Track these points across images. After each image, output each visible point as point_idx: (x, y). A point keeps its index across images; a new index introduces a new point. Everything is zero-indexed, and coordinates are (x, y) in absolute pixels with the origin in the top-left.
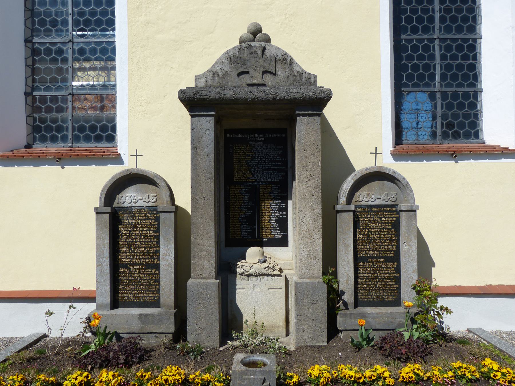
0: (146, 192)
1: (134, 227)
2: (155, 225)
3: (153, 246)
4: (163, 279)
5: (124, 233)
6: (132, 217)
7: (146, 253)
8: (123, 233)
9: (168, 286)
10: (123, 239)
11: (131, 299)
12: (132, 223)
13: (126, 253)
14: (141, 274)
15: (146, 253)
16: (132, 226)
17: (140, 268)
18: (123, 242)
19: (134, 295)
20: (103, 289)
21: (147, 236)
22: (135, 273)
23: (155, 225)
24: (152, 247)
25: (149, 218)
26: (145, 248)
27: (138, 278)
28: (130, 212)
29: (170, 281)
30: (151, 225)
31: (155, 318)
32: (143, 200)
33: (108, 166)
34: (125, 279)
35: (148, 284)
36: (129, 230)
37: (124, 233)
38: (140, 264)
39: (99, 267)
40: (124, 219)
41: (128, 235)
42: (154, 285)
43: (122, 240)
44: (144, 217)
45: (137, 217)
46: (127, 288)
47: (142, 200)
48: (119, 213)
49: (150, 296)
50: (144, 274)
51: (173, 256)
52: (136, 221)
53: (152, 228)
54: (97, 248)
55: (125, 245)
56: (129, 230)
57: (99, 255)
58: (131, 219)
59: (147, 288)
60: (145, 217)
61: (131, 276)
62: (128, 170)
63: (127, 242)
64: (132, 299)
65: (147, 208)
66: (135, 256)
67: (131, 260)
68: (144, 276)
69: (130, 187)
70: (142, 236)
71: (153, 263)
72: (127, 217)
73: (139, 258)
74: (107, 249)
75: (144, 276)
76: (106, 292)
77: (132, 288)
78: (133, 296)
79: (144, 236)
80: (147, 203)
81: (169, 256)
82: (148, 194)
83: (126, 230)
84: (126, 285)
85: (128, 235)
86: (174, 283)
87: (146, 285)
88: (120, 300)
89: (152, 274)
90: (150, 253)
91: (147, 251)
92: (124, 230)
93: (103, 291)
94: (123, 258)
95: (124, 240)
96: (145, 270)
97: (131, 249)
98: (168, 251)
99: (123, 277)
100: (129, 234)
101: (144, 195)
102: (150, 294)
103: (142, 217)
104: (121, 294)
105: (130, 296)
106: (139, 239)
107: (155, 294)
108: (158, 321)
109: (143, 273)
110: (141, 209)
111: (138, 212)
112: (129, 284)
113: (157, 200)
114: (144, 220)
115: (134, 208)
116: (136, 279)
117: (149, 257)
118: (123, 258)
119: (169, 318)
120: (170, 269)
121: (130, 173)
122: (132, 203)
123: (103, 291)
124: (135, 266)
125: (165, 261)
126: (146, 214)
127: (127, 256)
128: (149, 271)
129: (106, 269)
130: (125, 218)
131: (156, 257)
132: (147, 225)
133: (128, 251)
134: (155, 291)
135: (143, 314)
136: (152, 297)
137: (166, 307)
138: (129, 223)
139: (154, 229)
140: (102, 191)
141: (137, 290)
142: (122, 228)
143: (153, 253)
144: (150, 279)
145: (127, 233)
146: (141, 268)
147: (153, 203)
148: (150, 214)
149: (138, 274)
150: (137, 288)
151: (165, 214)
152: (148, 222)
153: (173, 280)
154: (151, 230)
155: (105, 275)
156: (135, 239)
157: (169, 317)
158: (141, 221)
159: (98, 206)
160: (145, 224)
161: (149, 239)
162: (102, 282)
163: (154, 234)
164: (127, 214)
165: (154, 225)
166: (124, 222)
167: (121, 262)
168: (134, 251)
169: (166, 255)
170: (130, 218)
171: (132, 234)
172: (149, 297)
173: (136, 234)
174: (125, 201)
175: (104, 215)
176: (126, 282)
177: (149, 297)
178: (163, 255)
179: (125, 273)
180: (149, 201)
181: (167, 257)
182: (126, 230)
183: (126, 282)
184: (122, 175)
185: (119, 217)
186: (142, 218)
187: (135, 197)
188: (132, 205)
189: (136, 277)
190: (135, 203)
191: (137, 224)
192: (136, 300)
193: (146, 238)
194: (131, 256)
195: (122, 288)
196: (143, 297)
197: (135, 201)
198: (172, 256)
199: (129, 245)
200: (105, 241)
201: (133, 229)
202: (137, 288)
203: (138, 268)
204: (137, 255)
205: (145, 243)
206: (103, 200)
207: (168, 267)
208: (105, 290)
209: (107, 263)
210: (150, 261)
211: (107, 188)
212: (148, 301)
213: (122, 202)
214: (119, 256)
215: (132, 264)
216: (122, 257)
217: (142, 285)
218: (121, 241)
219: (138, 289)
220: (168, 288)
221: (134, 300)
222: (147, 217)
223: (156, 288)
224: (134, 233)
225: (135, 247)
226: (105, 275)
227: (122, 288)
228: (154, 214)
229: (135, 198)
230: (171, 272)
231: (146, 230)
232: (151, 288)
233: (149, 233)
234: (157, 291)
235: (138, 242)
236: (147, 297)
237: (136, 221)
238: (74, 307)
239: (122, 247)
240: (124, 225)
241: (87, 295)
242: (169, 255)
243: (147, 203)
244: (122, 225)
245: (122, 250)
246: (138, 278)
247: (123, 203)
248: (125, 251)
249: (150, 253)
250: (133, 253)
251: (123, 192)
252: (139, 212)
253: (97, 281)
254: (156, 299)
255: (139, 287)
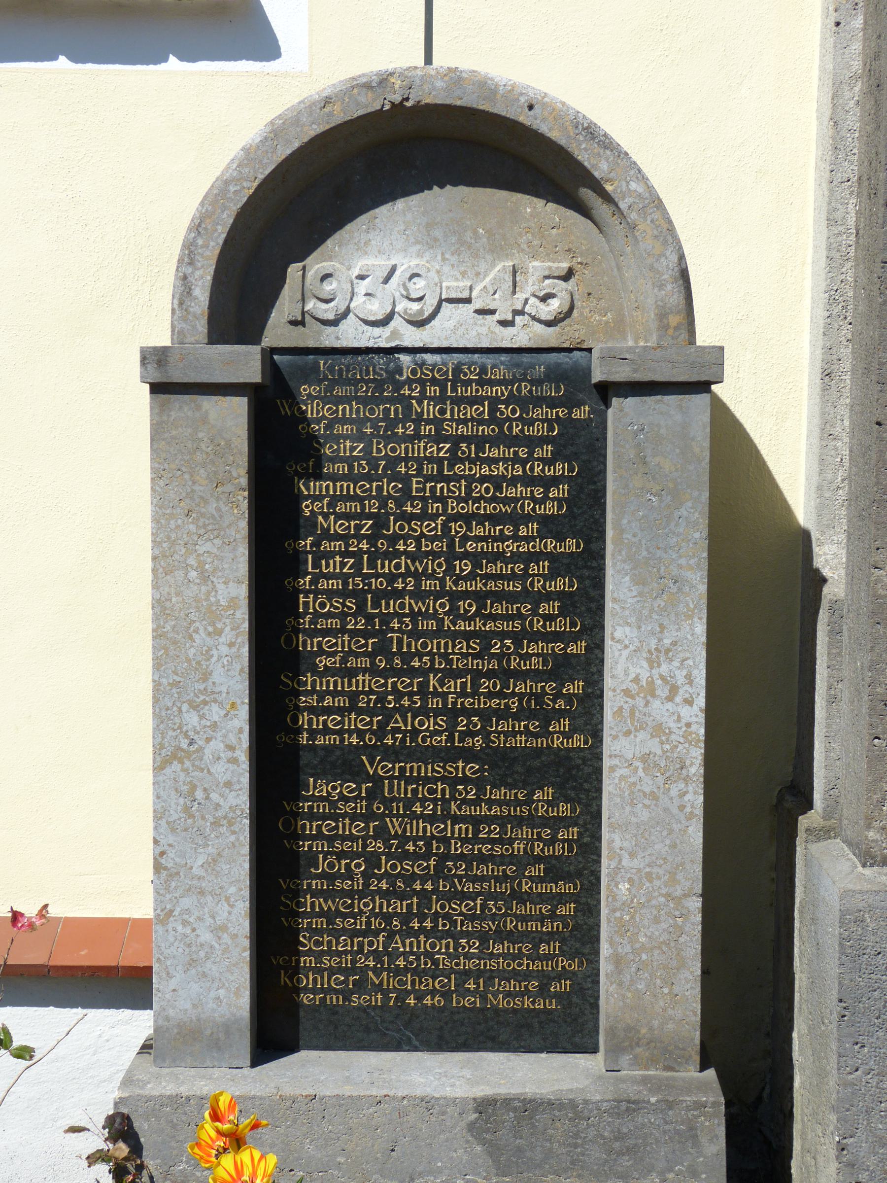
0: (498, 250)
1: (406, 495)
2: (555, 481)
3: (538, 626)
4: (625, 862)
5: (337, 537)
6: (392, 424)
7: (490, 674)
8: (326, 535)
9: (659, 908)
10: (328, 576)
11: (379, 988)
12: (393, 462)
13: (351, 673)
14: (456, 820)
15: (490, 674)
16: (389, 488)
17: (443, 779)
18: (330, 594)
19: (401, 963)
20: (199, 919)
21: (498, 556)
22: (414, 816)
23: (555, 481)
24: (535, 637)
25: (516, 431)
26: (486, 638)
27: (429, 845)
28: (379, 385)
29: (673, 874)
30: (529, 481)
31: (592, 1133)
32: (477, 304)
33: (163, 66)
34: (341, 855)
35: (505, 888)
36: (369, 516)
37: (337, 537)
38: (449, 755)
39: (176, 766)
40: (337, 439)
41: (364, 546)
42: (542, 898)
43: (323, 584)
44: (481, 422)
45: (428, 422)
46: (354, 916)
47: (468, 301)
48: (305, 390)
49: (515, 975)
50: (477, 821)
51: (701, 701)
52: (420, 449)
53: (533, 498)
54: (158, 634)
55: (343, 616)
56: (369, 516)
57: (175, 684)
58: (388, 439)
59: (493, 917)
60: (488, 423)
61: (382, 833)
62: (384, 79)
63: (359, 595)
64: (386, 993)
65: (504, 357)
66: (411, 694)
67: (382, 725)
68: (476, 832)
69: (383, 211)
70: (466, 555)
71: (541, 742)
72: (360, 422)
73: (437, 713)
74: (231, 645)
75: (476, 832)
76: (226, 939)
77: (388, 918)
78: (398, 971)
79: (476, 558)
80: (504, 323)
81: (670, 699)
82: (507, 256)
83: (348, 517)
84: (350, 894)
85: (364, 546)
86: (699, 889)
87: (490, 896)
88: (305, 999)
89: (531, 821)
90: (520, 675)
91: (494, 665)
92: (338, 517)
93: (206, 936)
94: (328, 711)
95: (335, 584)
96: (481, 790)
97: (383, 648)
98: (664, 669)
99: (331, 840)
100: (372, 539)
101: (482, 266)
102: (514, 957)
103: (465, 422)
104: (310, 952)
105: (377, 972)
106: (442, 581)
107: (548, 957)
108: (610, 1152)
109: (466, 811)
110: (457, 370)
111: (433, 391)
112: (366, 885)
113: (572, 308)
114: (480, 442)
115: (405, 359)
116: (416, 856)
117: (514, 708)
118: (328, 711)
119: (692, 1135)
120: (674, 792)
121: (397, 98)
122: (393, 324)
123: (206, 936)
124: (413, 768)
125: (642, 735)
126: (494, 402)
127: (354, 697)
128: (507, 803)
129: (228, 784)
130: (346, 429)
131: (561, 704)
132: (497, 482)
133: (364, 662)
134: (551, 936)
135: (507, 1102)
136: (527, 976)
137: (638, 1050)
138: (373, 463)
139: (551, 509)
140: (198, 227)
141: (422, 930)
142: (320, 498)
143: (536, 675)
144: (512, 859)
145: (359, 537)
146: (455, 781)
147: (549, 324)
148: (523, 403)
149: (432, 819)
150: (422, 918)
151: (651, 400)
152: (505, 460)
153: (696, 870)
154: (527, 519)
155: (216, 824)
156: (416, 575)
157: (691, 1129)
158: (455, 447)
159: (163, 339)
160: (485, 471)
161: (513, 577)
162: (196, 871)
163: (551, 545)
164: (359, 400)
165: (549, 483)
166: (333, 460)
167: (313, 733)
168: (407, 657)
169: (651, 691)
170: (376, 427)
171: (393, 539)
172: (507, 976)
173: (418, 540)
174: (348, 311)
175: (212, 405)
176: (349, 875)
177: (507, 976)
178: (627, 693)
179: (343, 809)
180: (516, 313)
181: (659, 709)
182: (348, 517)
183: (349, 875)
184: (339, 115)
185: (303, 418)
186: (462, 430)
187: (420, 283)
188: (395, 334)
189: (415, 839)
190: (420, 323)
191: (430, 469)
192: (419, 999)
193: (491, 569)
194: (381, 699)
195: (322, 914)
196: (466, 974)
197: (415, 307)
198: (689, 702)
199: (370, 618)
200: (220, 587)
201: (399, 504)
202: (422, 918)
203: (435, 780)
204: (424, 686)
205: (482, 606)
206: (202, 294)
207: (660, 780)
208: (219, 930)
209: (232, 739)
210: (514, 734)
211: (235, 207)
212: (502, 1002)
213: (327, 311)
214: (297, 694)
215: (392, 754)
216: (321, 699)
217: (463, 896)
218: (316, 592)
219: (428, 924)
220: (657, 920)
221: (403, 995)
222: (500, 424)
223: (553, 916)
224: (405, 538)
225: (415, 634)
226: (216, 824)
227: (322, 914)
228: (553, 403)
229: (418, 287)
230: (682, 808)
231: (494, 519)
232: (524, 919)
233: (516, 538)
234: (563, 941)
235: (438, 595)
236: (490, 976)
237: (420, 449)
238: (15, 1044)
239: (325, 632)
240: (334, 478)
241: (83, 957)
242: (674, 690)
243: (504, 323)
244: (318, 476)
245: (321, 652)
246: (429, 845)
247: (335, 323)
248: (344, 660)
249: (520, 675)
250: (399, 673)
251: (329, 243)
252: (443, 390)
253: (158, 867)
254: (558, 996)
255: (436, 907)
